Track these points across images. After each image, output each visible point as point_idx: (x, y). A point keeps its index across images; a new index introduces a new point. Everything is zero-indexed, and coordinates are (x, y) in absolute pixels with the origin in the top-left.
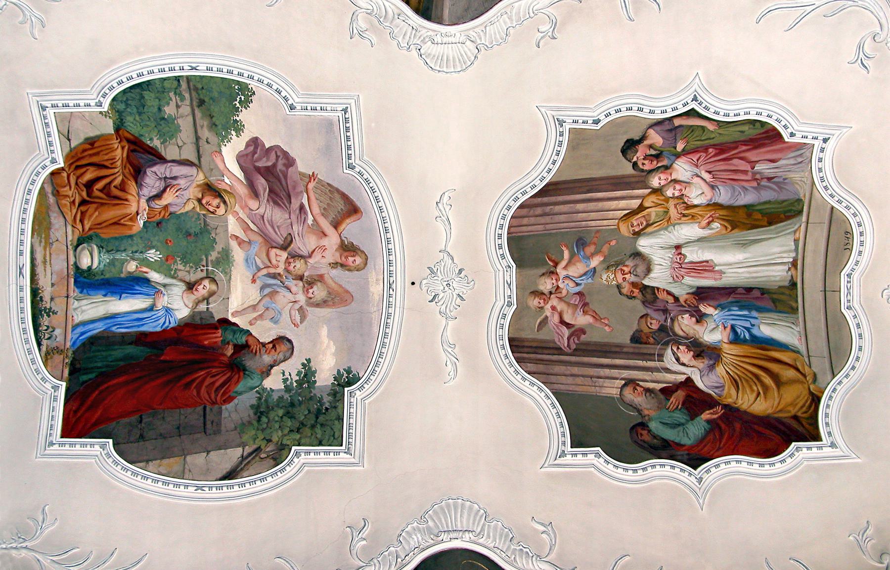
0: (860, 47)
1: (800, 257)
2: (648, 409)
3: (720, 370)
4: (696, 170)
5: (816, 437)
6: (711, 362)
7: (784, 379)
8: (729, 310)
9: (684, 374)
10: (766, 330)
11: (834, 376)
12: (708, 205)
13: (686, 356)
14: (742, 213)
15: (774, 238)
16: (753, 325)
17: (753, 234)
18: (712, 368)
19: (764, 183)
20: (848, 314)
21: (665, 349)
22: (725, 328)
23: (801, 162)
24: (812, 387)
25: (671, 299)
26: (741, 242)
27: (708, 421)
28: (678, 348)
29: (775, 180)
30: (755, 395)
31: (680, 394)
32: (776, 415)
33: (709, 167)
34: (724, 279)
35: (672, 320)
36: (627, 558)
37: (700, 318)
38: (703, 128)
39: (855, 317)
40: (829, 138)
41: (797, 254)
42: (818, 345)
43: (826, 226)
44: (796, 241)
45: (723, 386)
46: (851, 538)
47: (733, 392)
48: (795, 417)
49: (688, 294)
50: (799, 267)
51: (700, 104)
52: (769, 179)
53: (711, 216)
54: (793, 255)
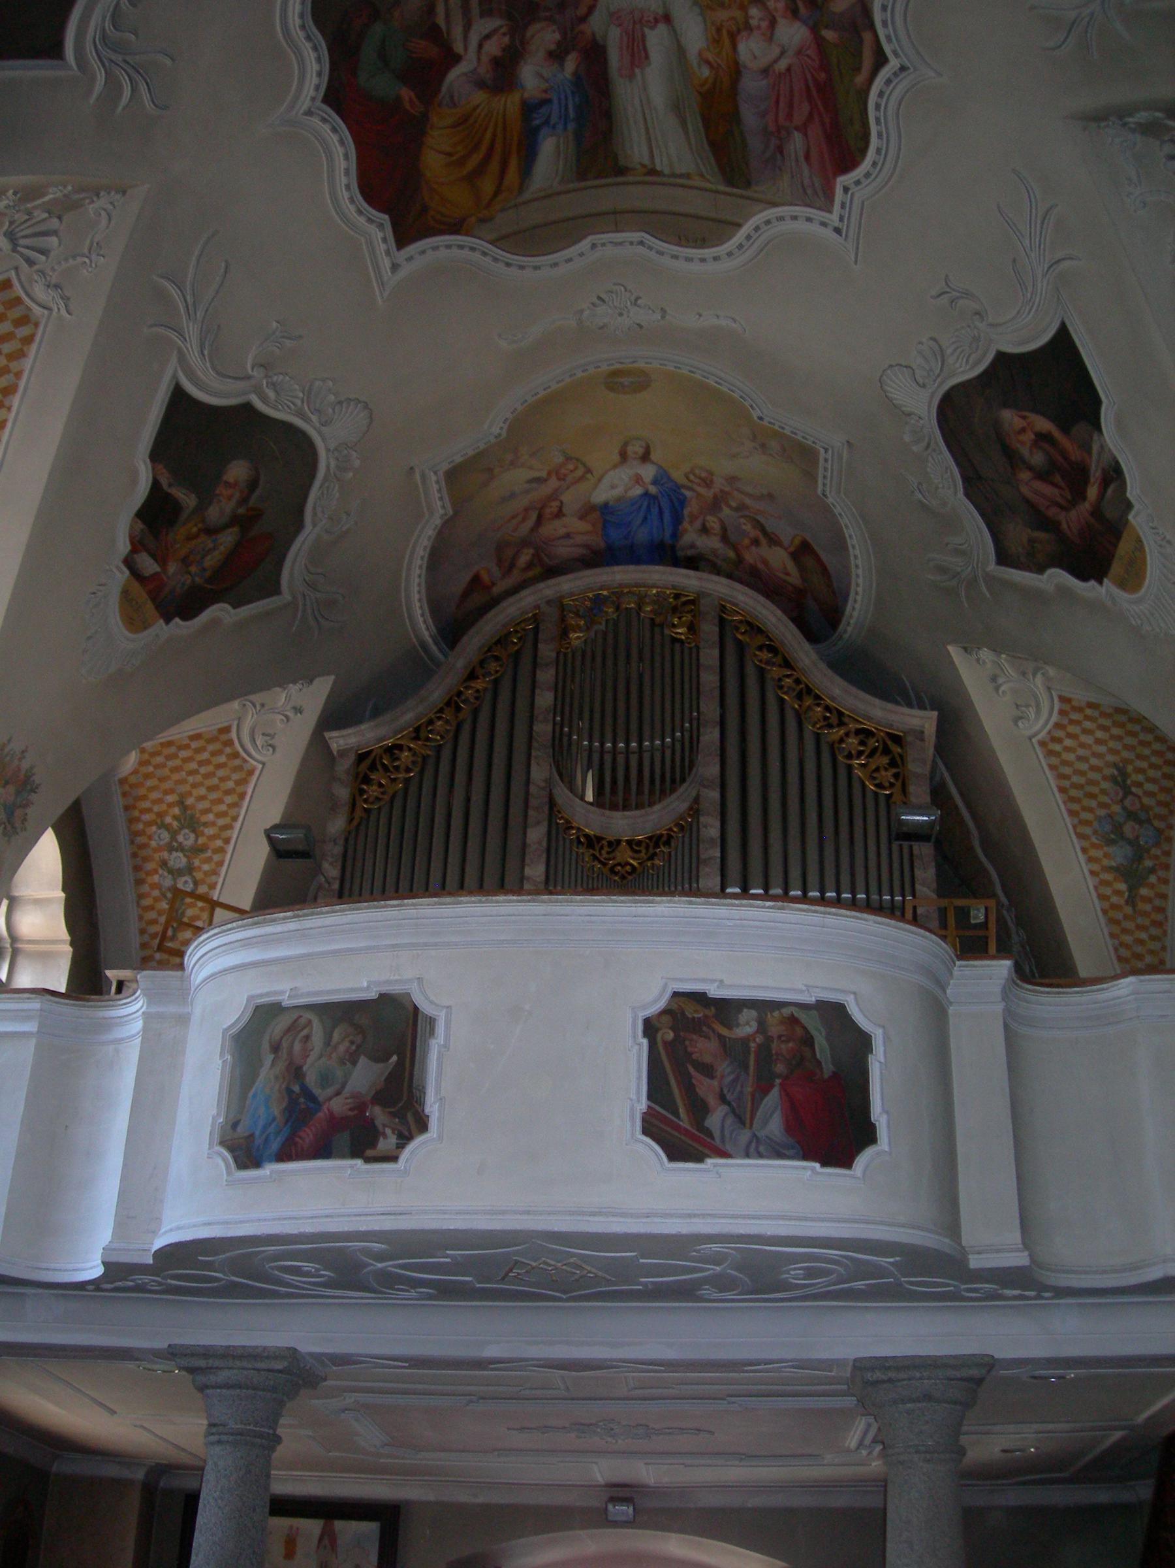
1: (665, 180)
3: (480, 97)
8: (573, 93)
10: (548, 147)
11: (492, 243)
13: (493, 48)
16: (554, 127)
18: (481, 85)
20: (585, 244)
22: (545, 91)
24: (473, 219)
25: (582, 11)
26: (694, 697)
28: (504, 34)
29: (779, 156)
30: (448, 149)
36: (168, 62)
37: (557, 56)
38: (858, 69)
39: (581, 255)
40: (841, 235)
44: (688, 176)
45: (455, 105)
46: (275, 324)
48: (425, 209)
49: (593, 35)
51: (895, 74)
52: (780, 149)
53: (718, 64)
54: (667, 171)
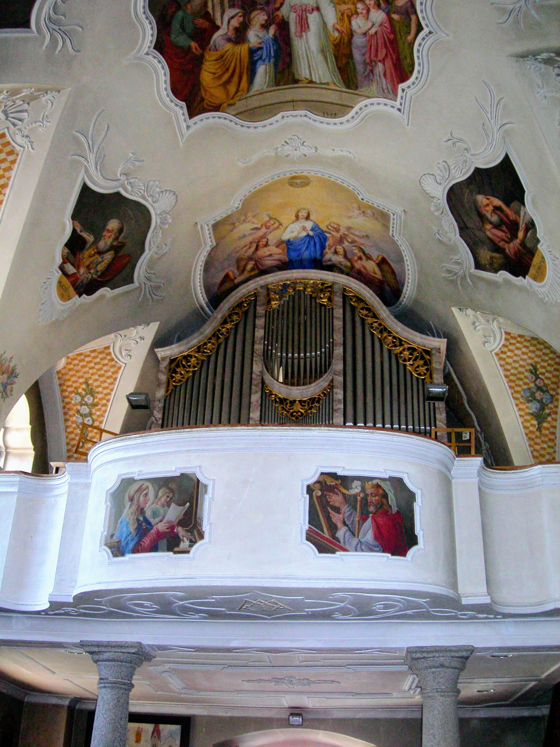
0: (461, 140)
2: (191, 7)
3: (229, 46)
4: (377, 25)
5: (191, 115)
6: (233, 39)
7: (228, 87)
8: (273, 44)
9: (222, 23)
12: (351, 30)
13: (235, 23)
14: (346, 51)
15: (329, 68)
16: (264, 61)
17: (331, 58)
18: (229, 40)
19: (369, 68)
20: (279, 116)
21: (239, 8)
22: (260, 43)
23: (384, 92)
24: (225, 104)
27: (190, 47)
28: (240, 16)
29: (371, 74)
30: (213, 71)
31: (205, 24)
32: (202, 87)
33: (380, 33)
34: (296, 38)
35: (261, 9)
36: (80, 29)
37: (265, 27)
38: (409, 33)
41: (318, 84)
42: (254, 102)
43: (340, 102)
44: (328, 84)
45: (217, 50)
46: (131, 154)
47: (214, 57)
48: (203, 99)
49: (283, 16)
50: (309, 85)
51: (427, 35)
52: (372, 71)
54: (318, 81)
